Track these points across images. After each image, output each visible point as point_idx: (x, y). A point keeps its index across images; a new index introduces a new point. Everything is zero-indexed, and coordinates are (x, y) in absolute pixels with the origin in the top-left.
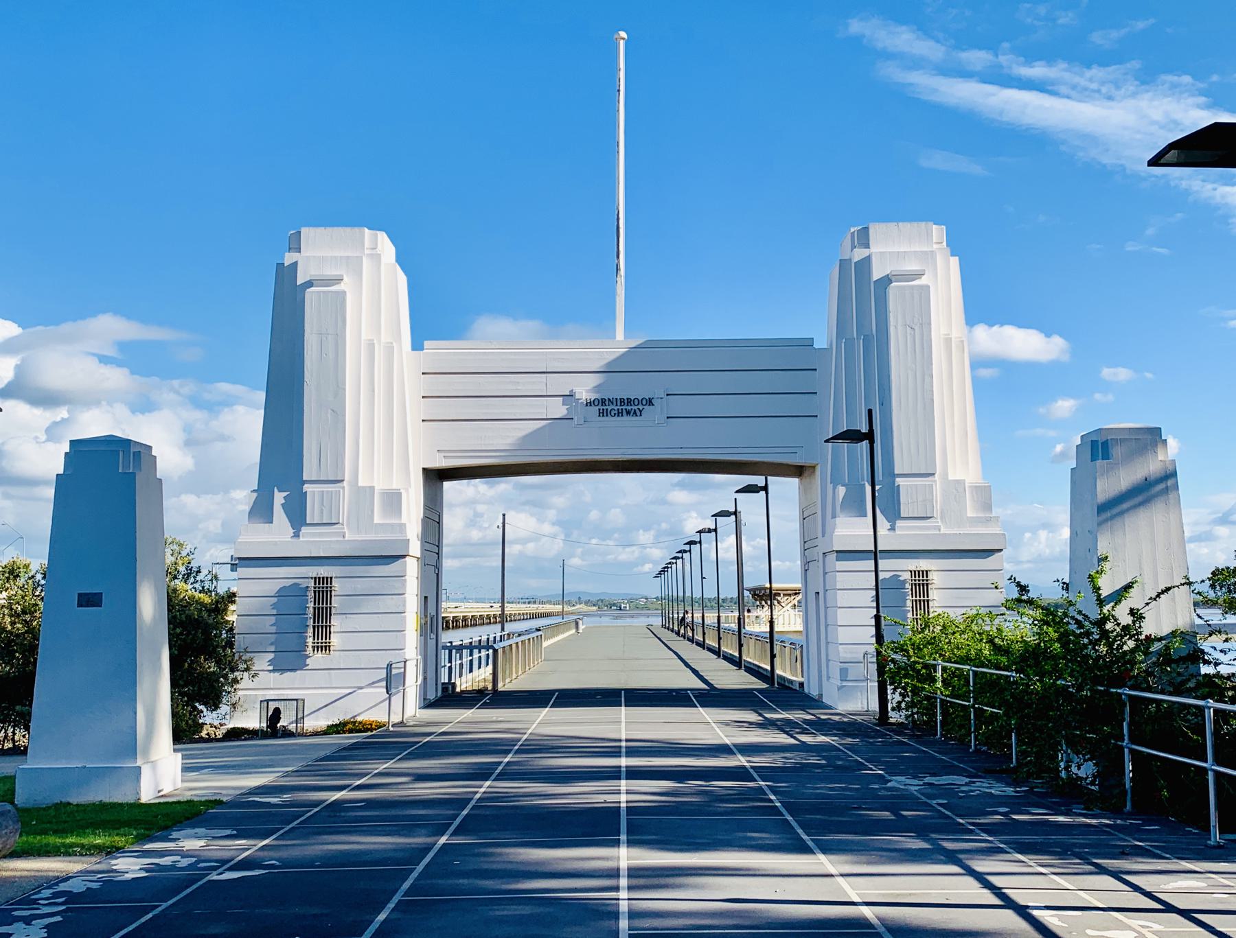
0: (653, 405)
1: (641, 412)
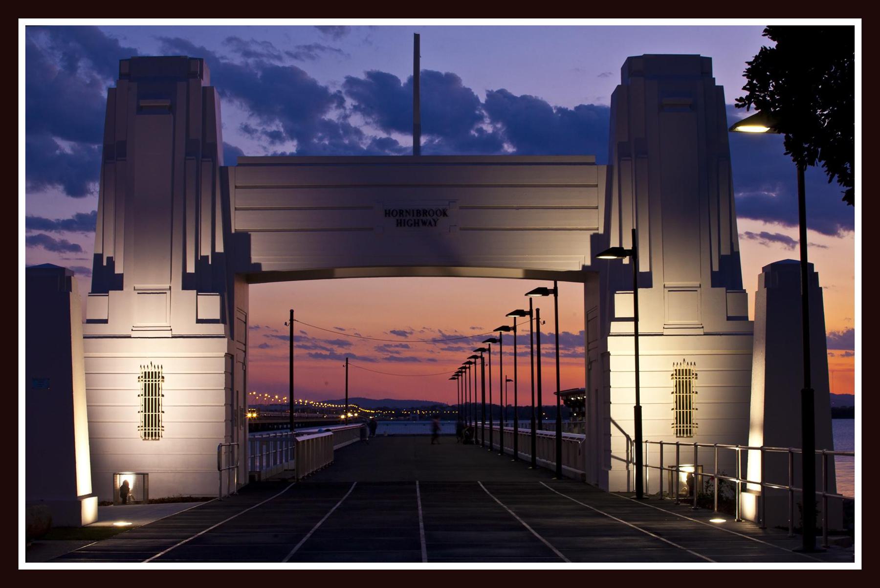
0: (447, 216)
1: (435, 222)
